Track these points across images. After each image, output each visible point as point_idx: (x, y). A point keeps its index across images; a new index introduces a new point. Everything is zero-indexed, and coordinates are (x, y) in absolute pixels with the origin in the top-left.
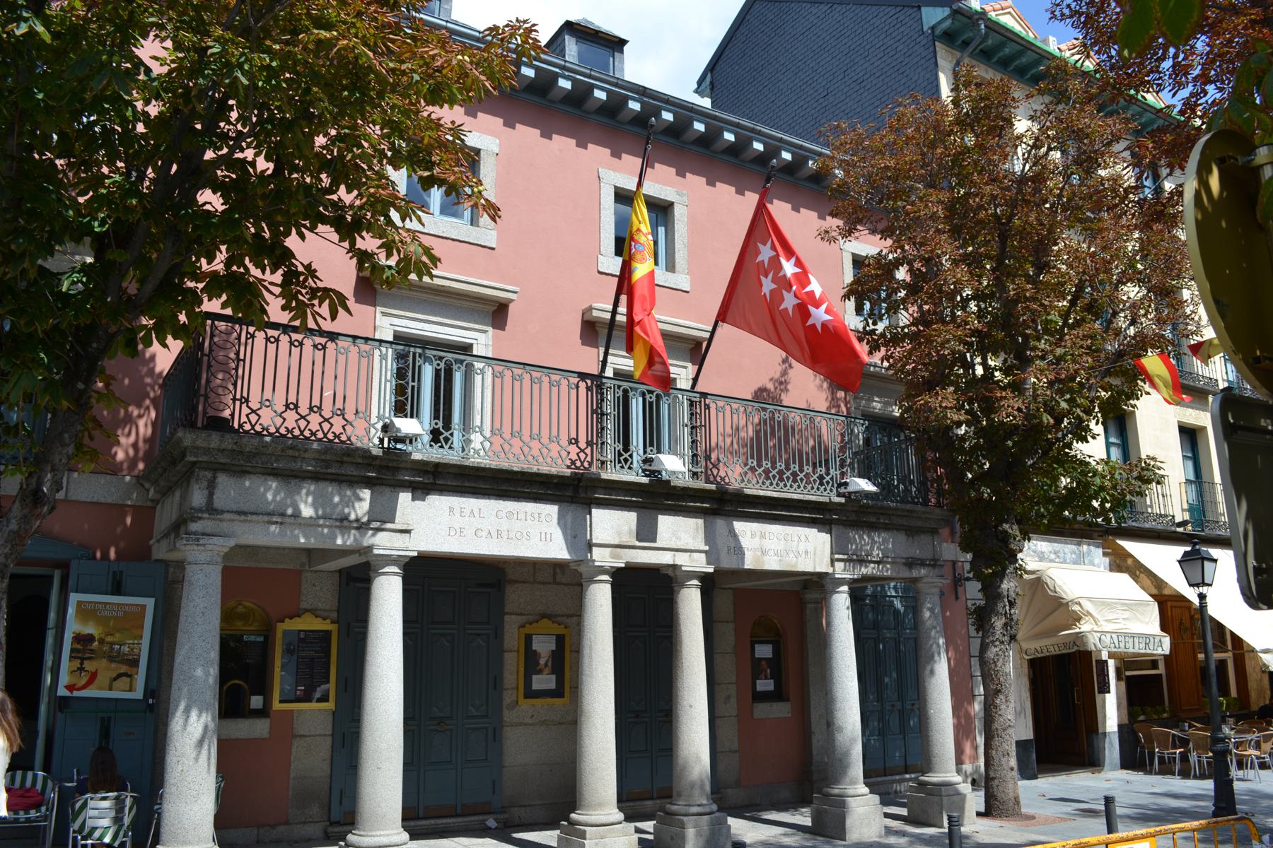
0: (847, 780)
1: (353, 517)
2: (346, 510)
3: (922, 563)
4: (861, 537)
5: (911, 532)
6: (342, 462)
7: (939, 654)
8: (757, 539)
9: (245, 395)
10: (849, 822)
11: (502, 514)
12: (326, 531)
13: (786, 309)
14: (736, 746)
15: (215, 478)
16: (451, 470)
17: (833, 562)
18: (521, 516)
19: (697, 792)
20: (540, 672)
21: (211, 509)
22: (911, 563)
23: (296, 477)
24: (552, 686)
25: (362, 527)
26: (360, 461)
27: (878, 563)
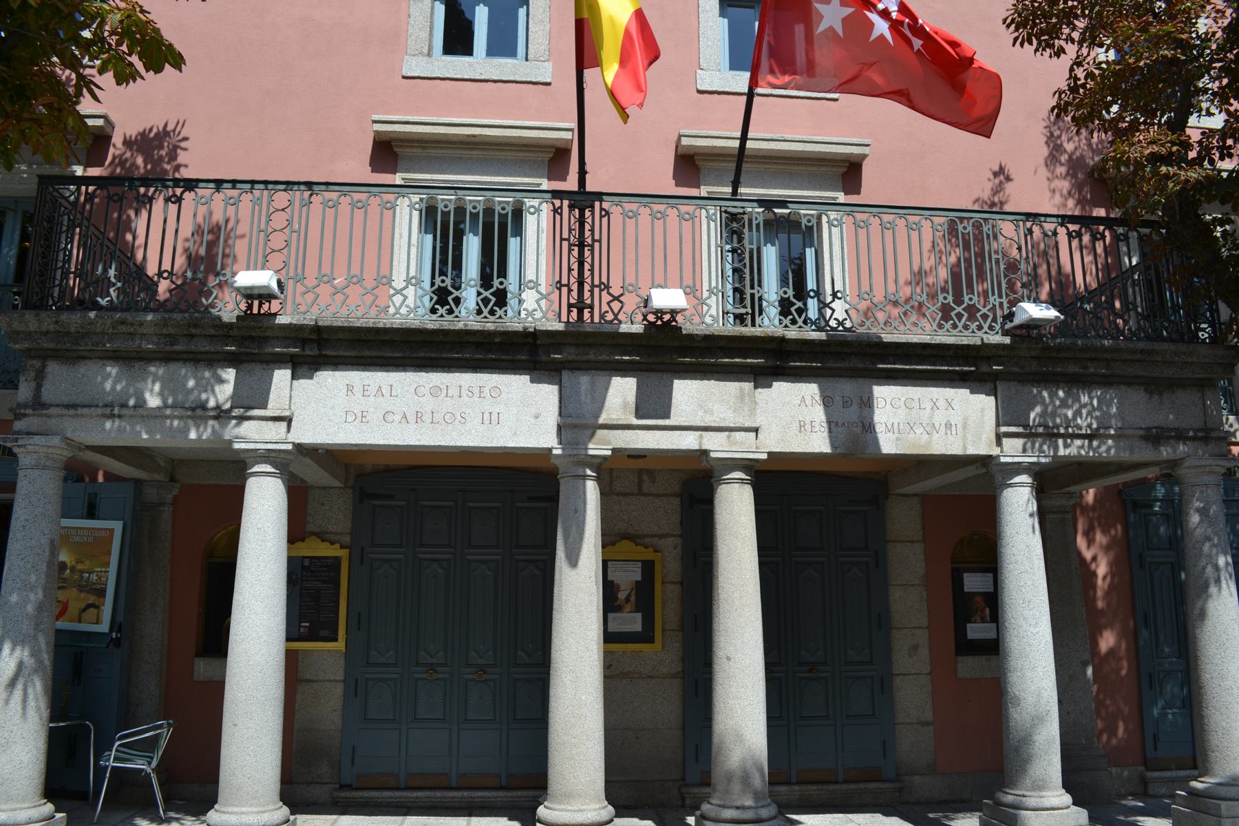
1: (212, 403)
2: (204, 396)
3: (1180, 436)
4: (1053, 395)
5: (1156, 386)
6: (192, 336)
7: (1218, 581)
8: (854, 408)
9: (604, 280)
11: (425, 390)
12: (176, 423)
13: (831, 29)
14: (928, 715)
15: (44, 366)
17: (999, 438)
18: (453, 391)
19: (736, 787)
20: (619, 609)
21: (38, 404)
22: (1155, 437)
23: (141, 359)
25: (221, 415)
26: (212, 332)
27: (1089, 438)
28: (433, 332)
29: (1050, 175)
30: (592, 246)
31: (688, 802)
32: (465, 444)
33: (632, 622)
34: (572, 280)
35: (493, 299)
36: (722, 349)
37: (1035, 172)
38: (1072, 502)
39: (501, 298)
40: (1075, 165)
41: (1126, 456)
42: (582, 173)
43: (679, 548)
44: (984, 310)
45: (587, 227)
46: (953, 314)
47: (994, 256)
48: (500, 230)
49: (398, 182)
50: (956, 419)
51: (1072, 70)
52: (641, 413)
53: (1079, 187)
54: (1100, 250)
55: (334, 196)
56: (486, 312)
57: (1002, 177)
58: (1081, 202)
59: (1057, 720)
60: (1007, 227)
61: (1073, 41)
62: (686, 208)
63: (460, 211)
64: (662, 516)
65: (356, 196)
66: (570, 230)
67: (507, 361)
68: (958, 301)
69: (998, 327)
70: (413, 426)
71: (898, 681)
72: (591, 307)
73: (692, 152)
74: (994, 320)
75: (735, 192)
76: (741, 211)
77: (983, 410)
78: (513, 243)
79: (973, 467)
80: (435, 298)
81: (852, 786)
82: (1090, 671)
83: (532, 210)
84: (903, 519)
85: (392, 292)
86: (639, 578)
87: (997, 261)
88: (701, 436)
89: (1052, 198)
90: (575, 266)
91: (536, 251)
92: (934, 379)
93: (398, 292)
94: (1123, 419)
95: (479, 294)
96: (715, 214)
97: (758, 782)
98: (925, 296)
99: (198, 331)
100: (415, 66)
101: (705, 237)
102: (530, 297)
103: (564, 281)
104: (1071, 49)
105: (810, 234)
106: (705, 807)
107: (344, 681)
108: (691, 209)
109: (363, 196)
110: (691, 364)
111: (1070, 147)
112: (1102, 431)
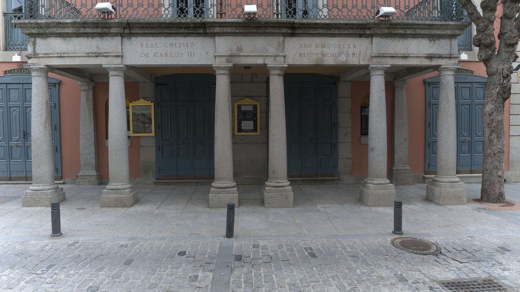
8: (320, 48)
9: (229, 3)
15: (35, 40)
18: (178, 45)
34: (275, 4)
35: (180, 11)
50: (357, 51)
56: (198, 16)
70: (164, 58)
77: (367, 48)
88: (264, 59)
99: (87, 26)
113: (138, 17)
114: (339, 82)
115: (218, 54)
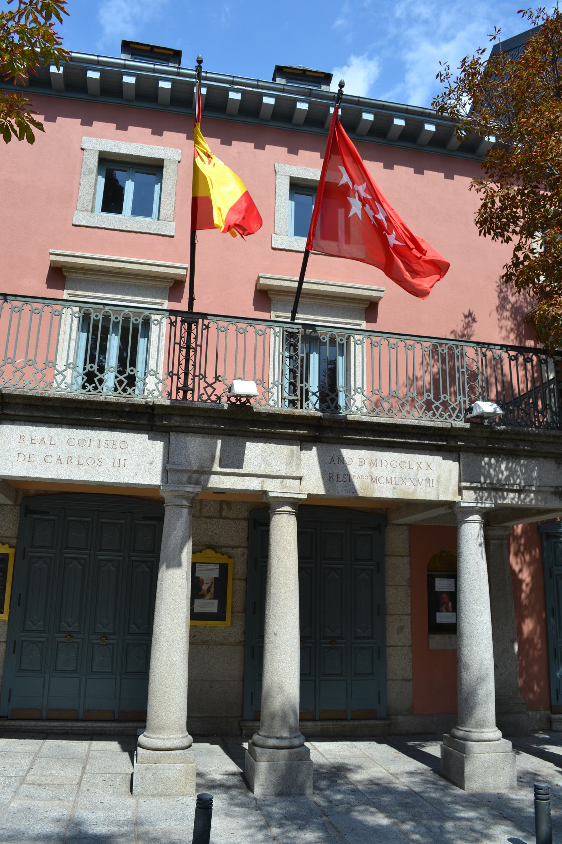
0: (473, 722)
8: (366, 466)
9: (202, 372)
10: (468, 769)
11: (75, 442)
14: (409, 675)
16: (18, 401)
17: (460, 490)
18: (94, 443)
19: (277, 723)
20: (202, 597)
24: (215, 609)
27: (519, 492)
28: (83, 402)
29: (499, 317)
30: (195, 349)
31: (244, 732)
32: (101, 480)
33: (210, 605)
35: (126, 382)
36: (280, 423)
37: (490, 315)
38: (507, 533)
39: (132, 380)
40: (516, 311)
41: (542, 505)
42: (191, 299)
43: (246, 556)
44: (454, 405)
45: (193, 336)
46: (433, 406)
47: (461, 370)
48: (133, 332)
49: (65, 297)
50: (433, 476)
51: (514, 253)
52: (223, 464)
53: (518, 326)
54: (529, 366)
55: (19, 304)
56: (120, 389)
57: (470, 319)
58: (518, 336)
59: (493, 680)
60: (470, 352)
61: (516, 233)
62: (260, 327)
63: (106, 318)
64: (235, 533)
65: (35, 305)
66: (181, 337)
67: (133, 424)
68: (437, 398)
69: (462, 416)
70: (64, 466)
71: (389, 651)
72: (193, 390)
73: (266, 288)
74: (460, 412)
75: (293, 318)
76: (297, 331)
77: (450, 471)
78: (142, 342)
79: (443, 508)
80: (86, 378)
81: (356, 723)
82: (516, 647)
83: (156, 322)
84: (397, 541)
85: (56, 372)
86: (217, 576)
87: (463, 373)
88: (263, 482)
89: (500, 332)
90: (183, 362)
91: (157, 349)
92: (419, 449)
93: (60, 373)
94: (540, 480)
95: (116, 377)
96: (279, 332)
97: (293, 720)
98: (415, 394)
100: (81, 218)
101: (272, 346)
102: (151, 382)
103: (175, 372)
104: (516, 239)
105: (344, 349)
106: (256, 737)
107: (6, 642)
108: (263, 328)
109: (40, 306)
110: (258, 432)
111: (512, 299)
112: (527, 488)
113: (21, 385)
114: (386, 526)
115: (174, 467)
